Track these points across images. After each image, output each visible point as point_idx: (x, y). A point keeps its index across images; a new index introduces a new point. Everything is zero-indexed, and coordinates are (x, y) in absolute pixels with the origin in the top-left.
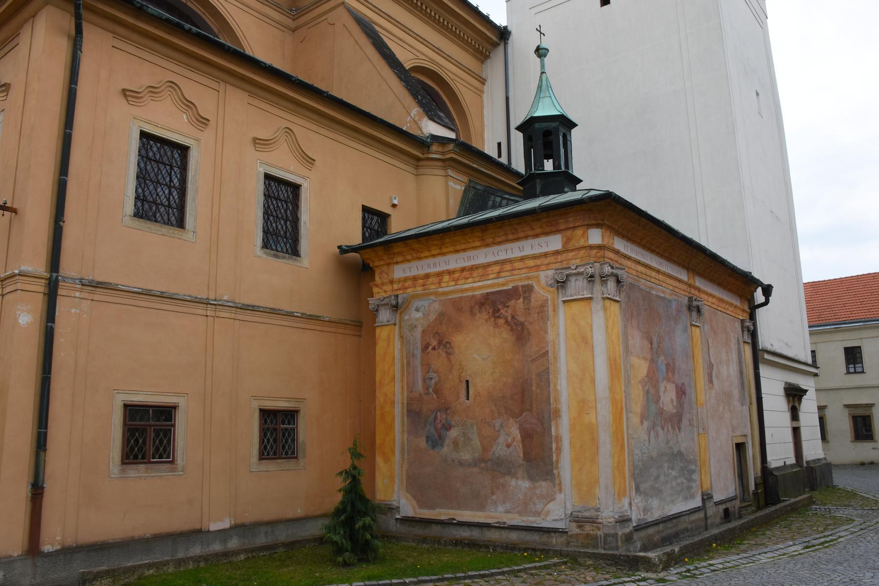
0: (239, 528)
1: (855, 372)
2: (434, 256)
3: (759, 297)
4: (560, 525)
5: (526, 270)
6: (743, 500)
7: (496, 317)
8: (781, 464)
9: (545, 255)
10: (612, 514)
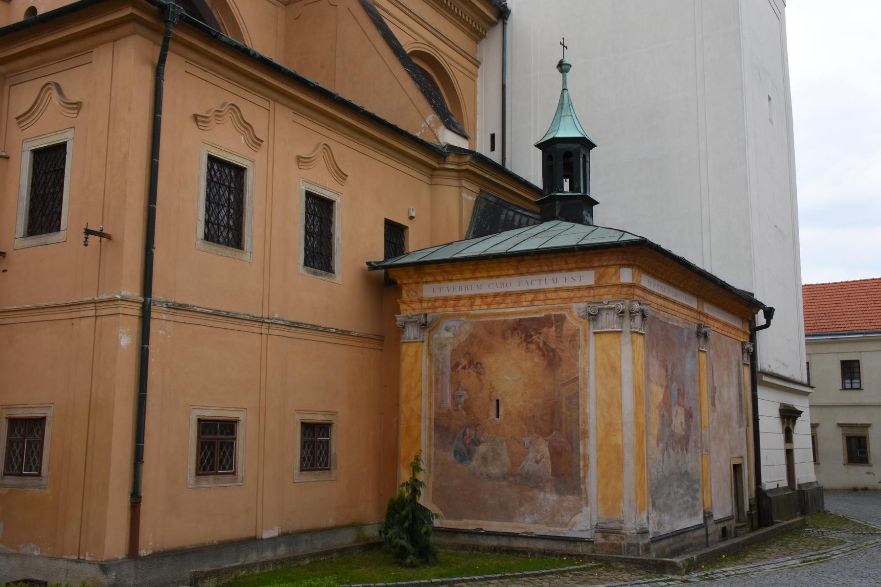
0: (286, 537)
1: (852, 389)
2: (466, 279)
3: (760, 318)
4: (586, 535)
5: (560, 301)
6: (738, 521)
7: (528, 343)
8: (774, 486)
9: (579, 288)
10: (634, 526)
